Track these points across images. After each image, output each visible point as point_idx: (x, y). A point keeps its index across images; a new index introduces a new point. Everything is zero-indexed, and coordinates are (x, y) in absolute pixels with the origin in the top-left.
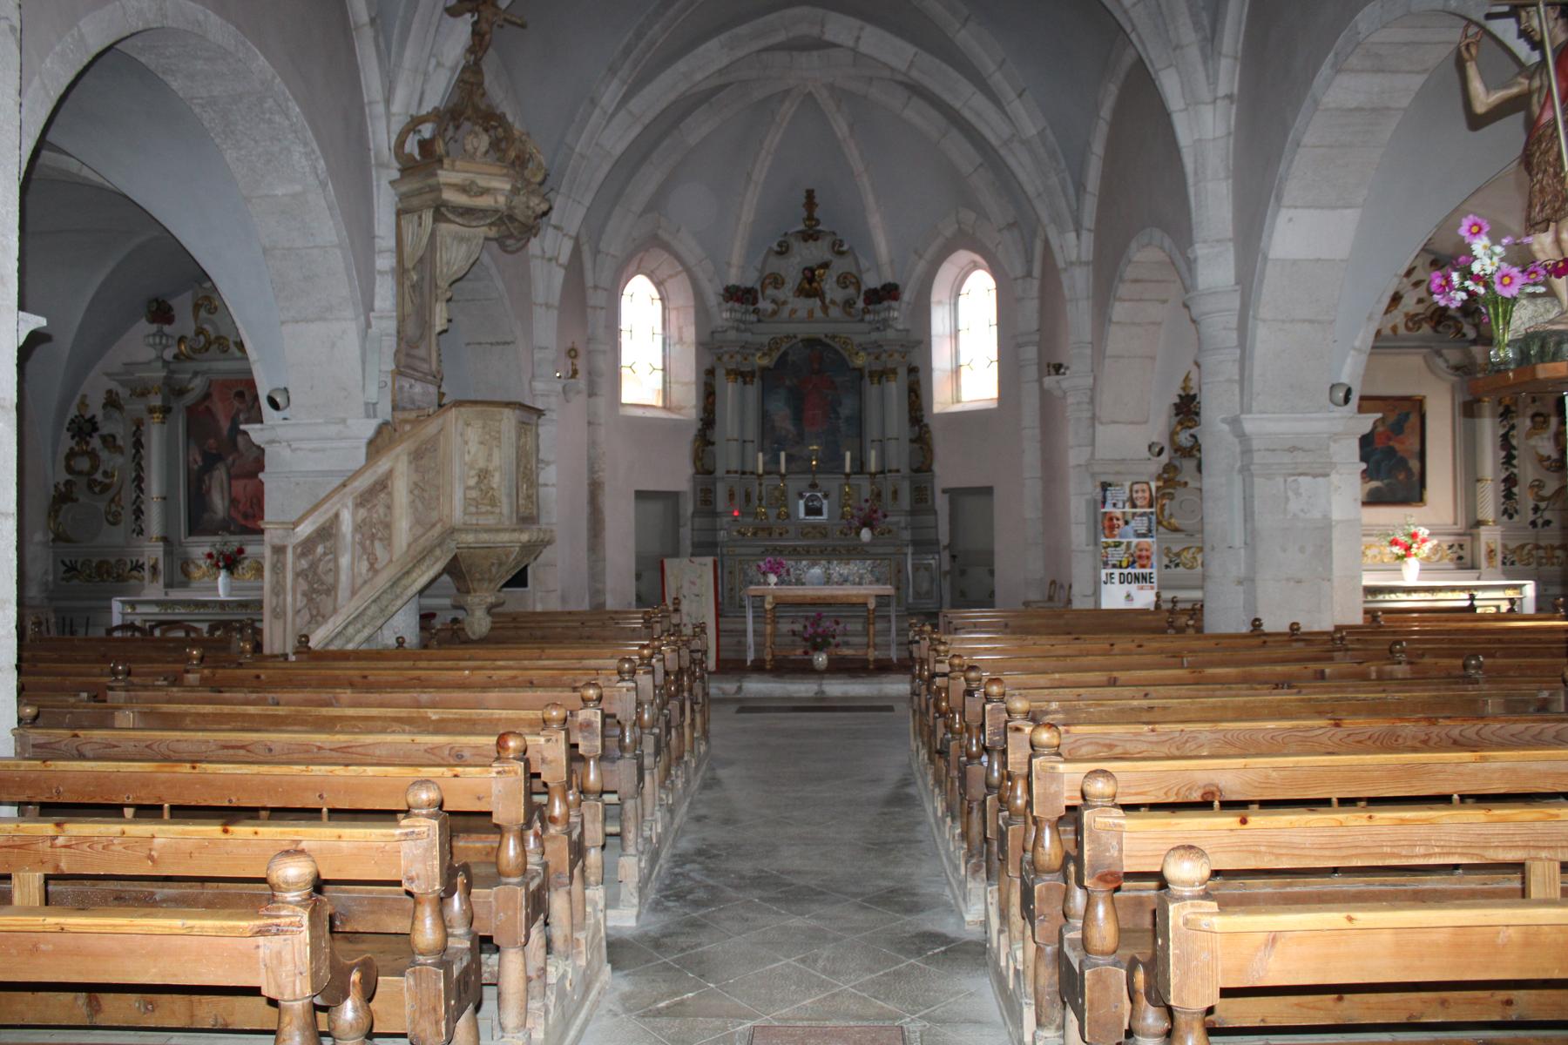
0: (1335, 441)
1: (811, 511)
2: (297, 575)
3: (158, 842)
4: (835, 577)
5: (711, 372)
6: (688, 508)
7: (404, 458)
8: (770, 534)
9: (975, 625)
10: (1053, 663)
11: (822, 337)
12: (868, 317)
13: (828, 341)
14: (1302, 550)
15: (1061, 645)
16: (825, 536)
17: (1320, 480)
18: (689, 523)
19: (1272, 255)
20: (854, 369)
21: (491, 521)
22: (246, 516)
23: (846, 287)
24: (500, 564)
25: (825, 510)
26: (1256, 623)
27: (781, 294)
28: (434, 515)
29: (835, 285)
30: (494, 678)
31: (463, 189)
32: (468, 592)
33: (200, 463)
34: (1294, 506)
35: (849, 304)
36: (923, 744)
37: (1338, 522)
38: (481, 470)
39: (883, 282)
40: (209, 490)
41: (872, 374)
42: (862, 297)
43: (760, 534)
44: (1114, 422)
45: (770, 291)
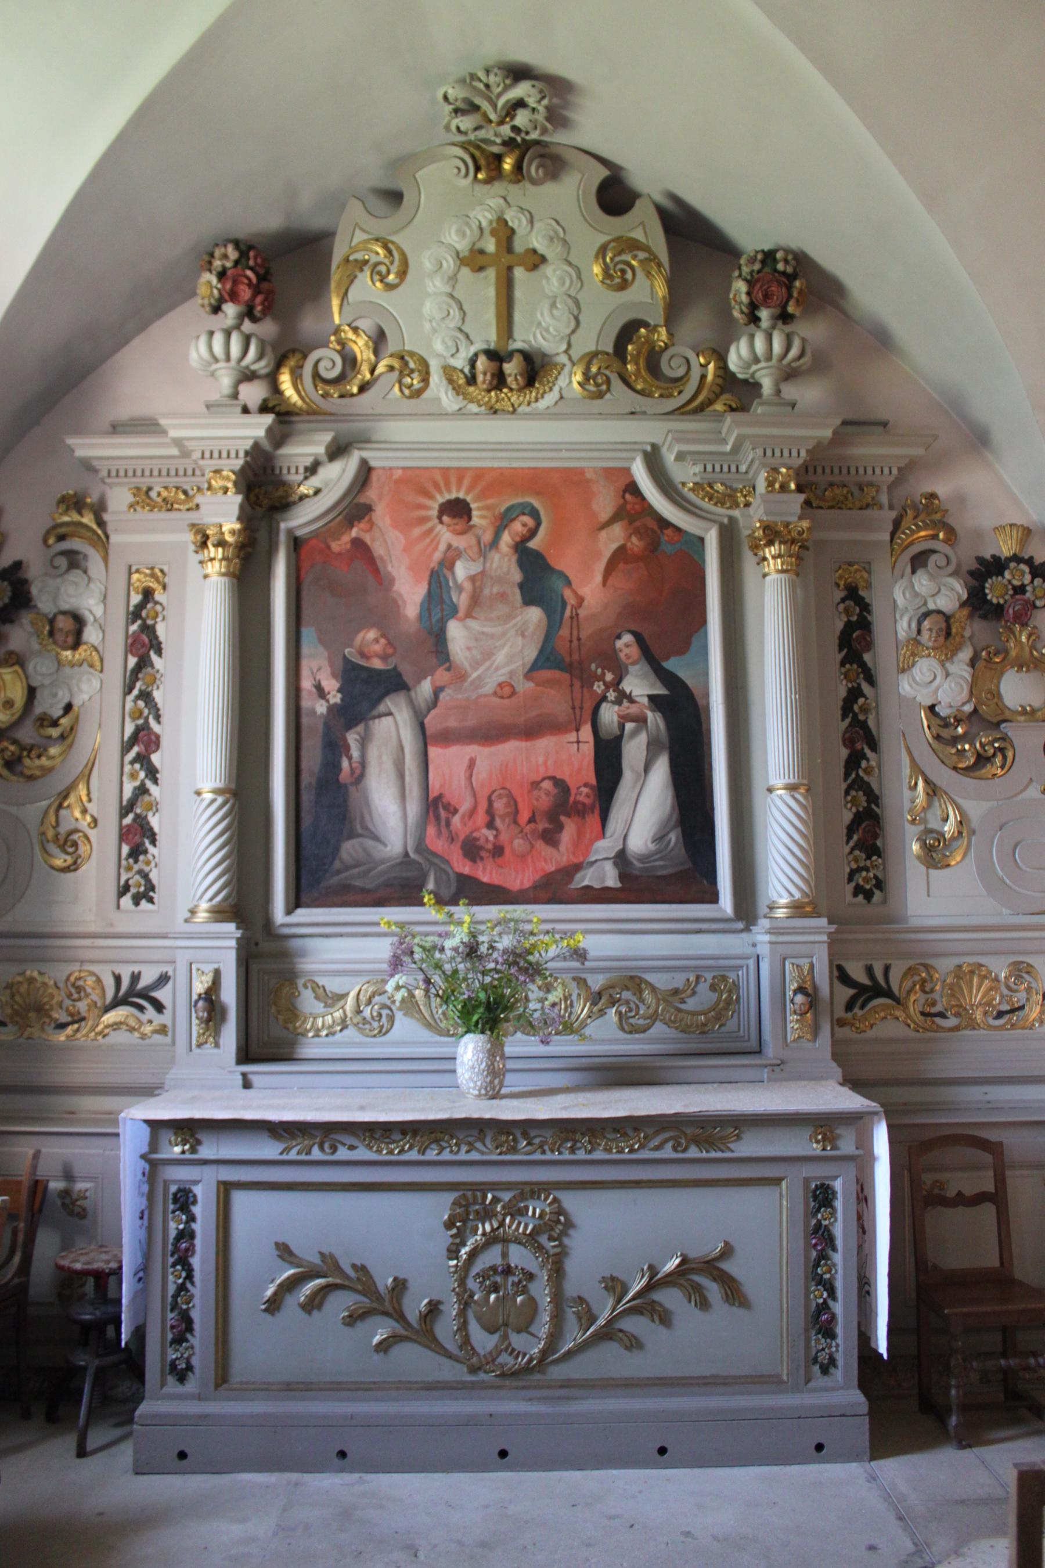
22: (472, 850)
33: (335, 698)
40: (360, 776)
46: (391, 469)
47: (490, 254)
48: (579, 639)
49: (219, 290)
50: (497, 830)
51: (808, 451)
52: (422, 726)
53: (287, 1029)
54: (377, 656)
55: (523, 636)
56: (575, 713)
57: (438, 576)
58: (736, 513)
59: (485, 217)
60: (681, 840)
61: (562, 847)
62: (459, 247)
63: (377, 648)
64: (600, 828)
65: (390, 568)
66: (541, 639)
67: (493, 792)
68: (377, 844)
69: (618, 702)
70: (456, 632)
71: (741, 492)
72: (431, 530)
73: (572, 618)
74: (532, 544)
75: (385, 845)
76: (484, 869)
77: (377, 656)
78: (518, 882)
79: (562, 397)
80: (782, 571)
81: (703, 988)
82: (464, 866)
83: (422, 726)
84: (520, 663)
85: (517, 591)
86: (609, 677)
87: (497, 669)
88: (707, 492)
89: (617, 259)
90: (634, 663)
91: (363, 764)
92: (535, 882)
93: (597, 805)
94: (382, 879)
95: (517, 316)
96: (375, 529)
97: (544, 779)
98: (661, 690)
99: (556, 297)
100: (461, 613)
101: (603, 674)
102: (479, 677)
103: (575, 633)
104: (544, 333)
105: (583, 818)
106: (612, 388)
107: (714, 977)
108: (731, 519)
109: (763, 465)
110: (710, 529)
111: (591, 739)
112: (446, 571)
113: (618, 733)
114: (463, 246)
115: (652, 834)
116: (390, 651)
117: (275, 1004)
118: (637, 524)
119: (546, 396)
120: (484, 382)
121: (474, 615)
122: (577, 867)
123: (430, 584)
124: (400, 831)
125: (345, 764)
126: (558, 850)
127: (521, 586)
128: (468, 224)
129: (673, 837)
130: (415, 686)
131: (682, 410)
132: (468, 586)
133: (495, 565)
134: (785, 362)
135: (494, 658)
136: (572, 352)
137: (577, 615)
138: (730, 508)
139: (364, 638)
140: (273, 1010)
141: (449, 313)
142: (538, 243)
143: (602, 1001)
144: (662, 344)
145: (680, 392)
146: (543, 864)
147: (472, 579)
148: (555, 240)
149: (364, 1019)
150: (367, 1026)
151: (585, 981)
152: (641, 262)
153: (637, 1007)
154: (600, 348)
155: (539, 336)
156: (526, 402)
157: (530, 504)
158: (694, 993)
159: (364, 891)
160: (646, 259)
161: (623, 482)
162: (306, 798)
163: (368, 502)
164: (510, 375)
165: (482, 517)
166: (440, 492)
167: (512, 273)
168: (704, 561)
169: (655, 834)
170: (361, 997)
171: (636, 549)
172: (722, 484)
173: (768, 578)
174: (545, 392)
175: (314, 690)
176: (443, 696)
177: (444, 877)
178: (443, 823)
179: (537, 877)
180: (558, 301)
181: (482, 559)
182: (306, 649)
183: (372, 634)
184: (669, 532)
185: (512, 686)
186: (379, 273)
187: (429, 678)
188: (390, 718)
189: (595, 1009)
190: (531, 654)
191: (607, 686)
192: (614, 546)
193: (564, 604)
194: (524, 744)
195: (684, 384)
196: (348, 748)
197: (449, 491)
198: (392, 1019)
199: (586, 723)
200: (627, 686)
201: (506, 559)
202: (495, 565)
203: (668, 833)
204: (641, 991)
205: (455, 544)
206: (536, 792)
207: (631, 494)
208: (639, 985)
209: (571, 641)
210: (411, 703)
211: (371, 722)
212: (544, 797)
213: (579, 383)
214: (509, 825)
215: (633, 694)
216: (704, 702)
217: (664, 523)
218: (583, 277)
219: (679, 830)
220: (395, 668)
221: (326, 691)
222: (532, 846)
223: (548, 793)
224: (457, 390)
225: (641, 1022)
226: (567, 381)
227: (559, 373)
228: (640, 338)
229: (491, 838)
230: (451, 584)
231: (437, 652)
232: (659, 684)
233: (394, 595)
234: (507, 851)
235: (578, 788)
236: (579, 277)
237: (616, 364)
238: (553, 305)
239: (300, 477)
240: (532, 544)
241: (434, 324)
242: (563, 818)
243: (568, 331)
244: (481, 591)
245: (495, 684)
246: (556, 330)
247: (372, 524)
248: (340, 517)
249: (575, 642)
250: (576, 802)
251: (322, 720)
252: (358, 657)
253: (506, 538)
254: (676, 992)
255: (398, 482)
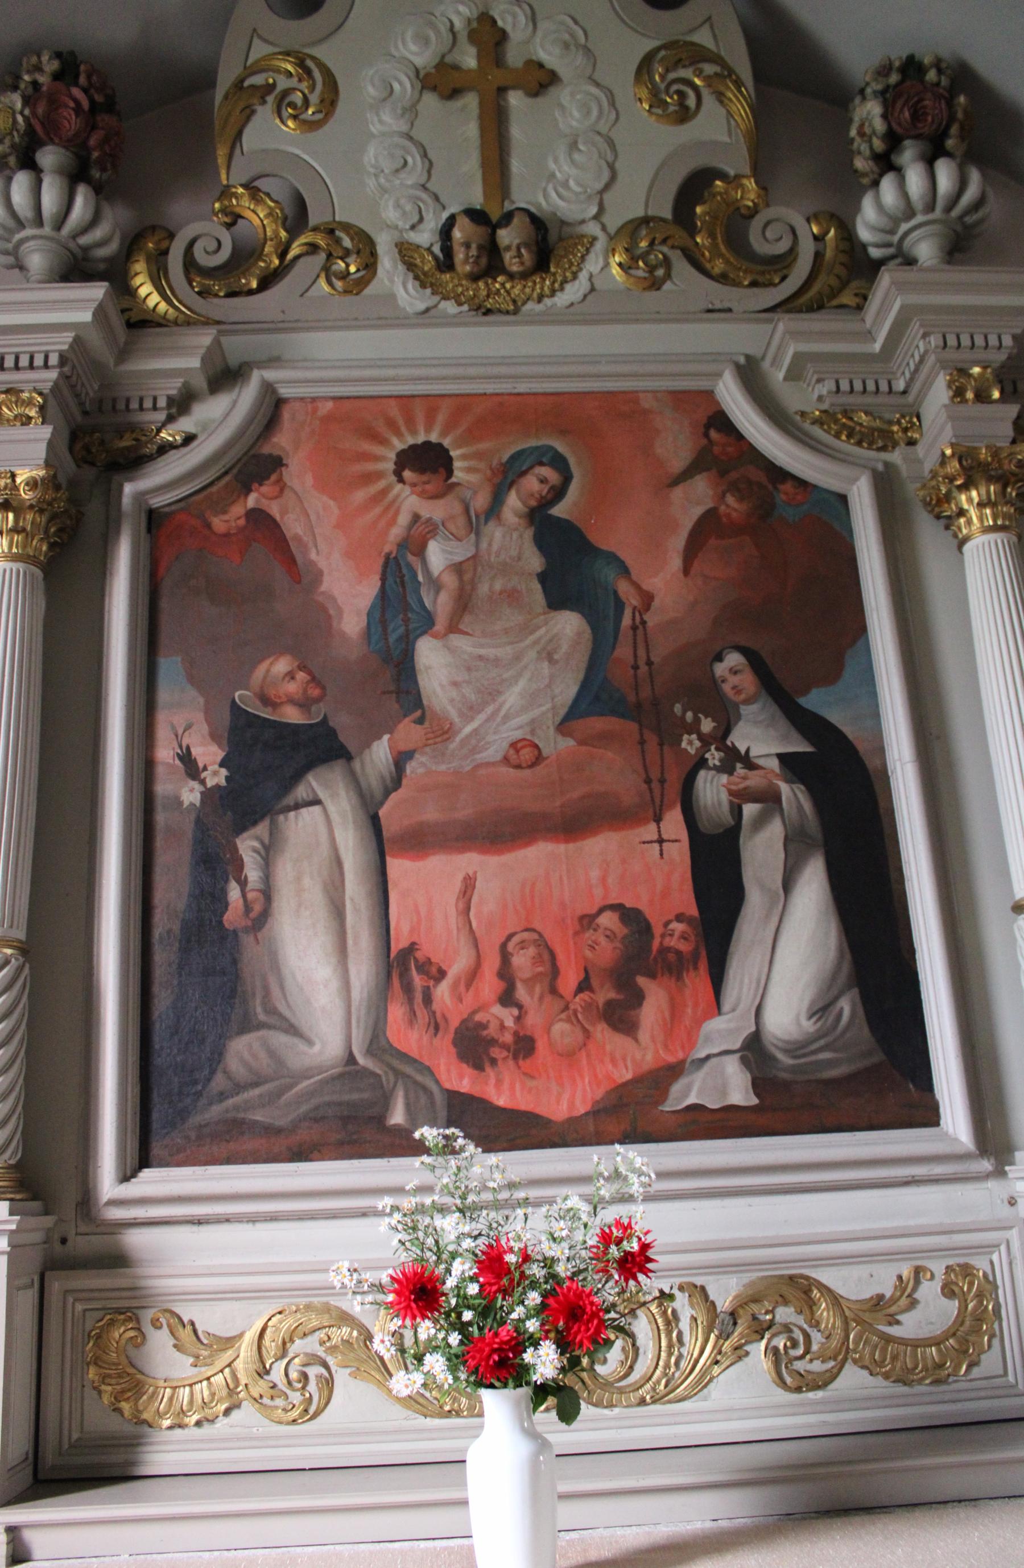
33: (217, 777)
46: (314, 400)
47: (470, 71)
48: (649, 663)
49: (26, 119)
50: (520, 1007)
51: (1015, 337)
52: (375, 821)
53: (118, 1411)
54: (291, 701)
55: (551, 660)
56: (651, 790)
57: (398, 565)
58: (895, 457)
59: (459, 13)
60: (861, 1012)
61: (644, 1035)
62: (419, 61)
63: (292, 688)
64: (713, 999)
65: (313, 556)
66: (583, 665)
67: (510, 937)
68: (296, 1040)
69: (726, 768)
71: (899, 423)
72: (384, 492)
73: (634, 628)
74: (559, 510)
75: (310, 1042)
76: (499, 1083)
77: (291, 701)
78: (564, 1105)
79: (593, 289)
80: (995, 529)
81: (929, 1291)
82: (461, 1077)
83: (375, 821)
84: (549, 706)
85: (537, 586)
86: (707, 725)
87: (507, 718)
88: (844, 424)
89: (672, 76)
90: (747, 702)
91: (267, 894)
92: (596, 1103)
93: (703, 953)
94: (304, 1108)
95: (516, 165)
96: (287, 493)
97: (601, 911)
98: (800, 746)
99: (577, 135)
100: (440, 626)
101: (697, 721)
102: (475, 731)
103: (642, 653)
104: (560, 190)
105: (679, 978)
106: (674, 273)
107: (949, 1269)
108: (887, 464)
109: (943, 364)
110: (856, 479)
111: (684, 835)
112: (410, 558)
113: (729, 820)
114: (423, 58)
115: (806, 1004)
116: (316, 692)
117: (96, 1362)
118: (734, 475)
119: (568, 287)
120: (466, 261)
121: (461, 627)
122: (674, 1071)
123: (383, 579)
124: (338, 1015)
125: (234, 893)
126: (636, 1040)
127: (543, 578)
128: (432, 25)
129: (846, 1006)
130: (361, 753)
131: (790, 306)
132: (450, 581)
133: (495, 547)
134: (955, 213)
135: (501, 699)
136: (606, 219)
137: (644, 623)
138: (883, 449)
139: (268, 671)
140: (92, 1373)
141: (406, 163)
142: (549, 56)
143: (739, 1330)
144: (750, 204)
145: (783, 279)
146: (610, 1067)
147: (458, 568)
148: (572, 47)
149: (274, 1386)
150: (279, 1402)
151: (703, 1289)
152: (707, 79)
153: (807, 1337)
154: (650, 213)
155: (553, 195)
156: (535, 295)
157: (551, 448)
158: (913, 1303)
159: (270, 1131)
160: (716, 74)
161: (702, 415)
162: (162, 958)
163: (276, 452)
164: (508, 248)
165: (469, 470)
166: (399, 434)
167: (505, 100)
168: (850, 532)
169: (813, 1003)
170: (267, 1341)
171: (734, 514)
172: (866, 413)
173: (967, 548)
174: (565, 281)
175: (177, 762)
176: (410, 768)
177: (423, 1100)
178: (419, 997)
179: (600, 1093)
180: (580, 141)
181: (473, 536)
182: (164, 695)
183: (282, 666)
184: (788, 487)
185: (536, 746)
186: (292, 105)
187: (386, 737)
188: (316, 809)
189: (727, 1346)
190: (567, 690)
191: (706, 741)
192: (698, 511)
193: (619, 605)
194: (562, 848)
195: (789, 266)
196: (239, 864)
197: (414, 432)
198: (328, 1384)
199: (671, 807)
200: (741, 739)
201: (515, 535)
202: (495, 547)
203: (836, 998)
204: (811, 1305)
205: (425, 514)
206: (589, 934)
207: (719, 430)
208: (807, 1292)
209: (636, 667)
211: (281, 817)
213: (620, 265)
214: (541, 998)
215: (753, 753)
216: (878, 762)
217: (779, 474)
218: (618, 105)
219: (855, 991)
220: (325, 721)
221: (201, 765)
222: (587, 1034)
223: (610, 936)
224: (423, 280)
225: (817, 1366)
226: (601, 263)
227: (588, 250)
228: (714, 196)
229: (509, 1023)
230: (420, 578)
231: (398, 692)
232: (795, 735)
233: (320, 599)
234: (541, 1045)
235: (666, 924)
236: (613, 104)
237: (680, 235)
238: (573, 146)
239: (161, 416)
240: (559, 510)
241: (382, 180)
242: (641, 981)
243: (599, 186)
244: (474, 588)
245: (505, 745)
246: (578, 184)
247: (282, 487)
248: (227, 478)
249: (643, 669)
250: (664, 950)
251: (193, 817)
252: (258, 703)
253: (513, 501)
254: (878, 1302)
255: (328, 419)
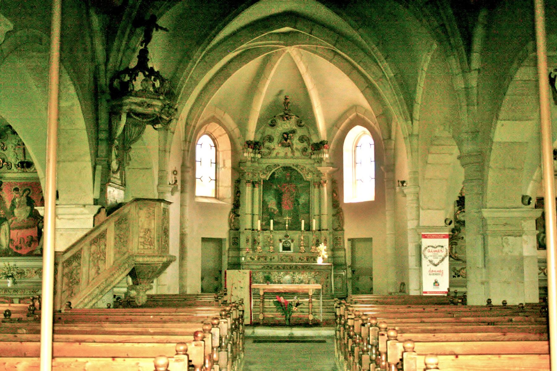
0: (525, 221)
1: (285, 248)
2: (63, 276)
3: (87, 365)
4: (297, 280)
5: (238, 181)
6: (227, 246)
7: (113, 224)
8: (266, 259)
9: (363, 301)
10: (399, 315)
11: (291, 166)
12: (313, 157)
13: (294, 168)
14: (510, 269)
15: (402, 309)
16: (292, 261)
17: (518, 238)
18: (227, 254)
19: (495, 140)
20: (306, 181)
21: (150, 252)
22: (17, 247)
23: (303, 142)
24: (153, 272)
25: (292, 248)
26: (489, 301)
27: (272, 145)
28: (124, 249)
29: (298, 141)
30: (163, 319)
31: (141, 104)
32: (138, 284)
34: (506, 249)
35: (305, 150)
36: (342, 353)
37: (527, 257)
38: (146, 229)
39: (320, 141)
41: (315, 183)
42: (310, 147)
43: (262, 259)
44: (429, 209)
45: (267, 144)
70: (16, 211)
176: (13, 222)
190: (28, 214)
210: (8, 223)
212: (29, 239)
